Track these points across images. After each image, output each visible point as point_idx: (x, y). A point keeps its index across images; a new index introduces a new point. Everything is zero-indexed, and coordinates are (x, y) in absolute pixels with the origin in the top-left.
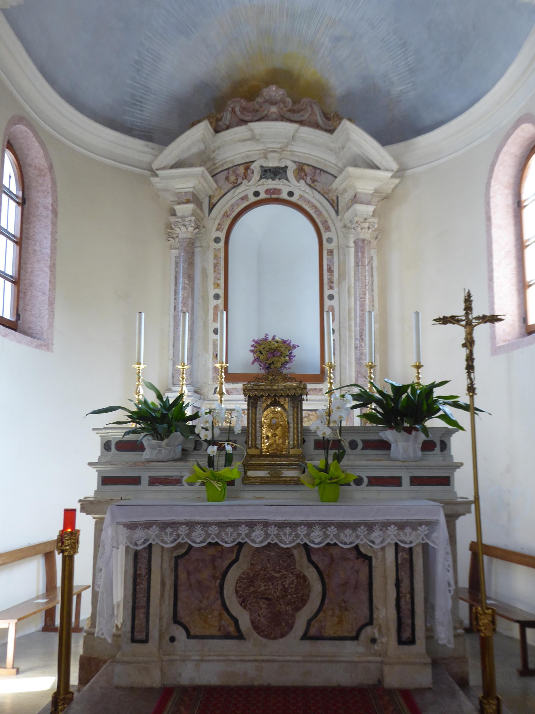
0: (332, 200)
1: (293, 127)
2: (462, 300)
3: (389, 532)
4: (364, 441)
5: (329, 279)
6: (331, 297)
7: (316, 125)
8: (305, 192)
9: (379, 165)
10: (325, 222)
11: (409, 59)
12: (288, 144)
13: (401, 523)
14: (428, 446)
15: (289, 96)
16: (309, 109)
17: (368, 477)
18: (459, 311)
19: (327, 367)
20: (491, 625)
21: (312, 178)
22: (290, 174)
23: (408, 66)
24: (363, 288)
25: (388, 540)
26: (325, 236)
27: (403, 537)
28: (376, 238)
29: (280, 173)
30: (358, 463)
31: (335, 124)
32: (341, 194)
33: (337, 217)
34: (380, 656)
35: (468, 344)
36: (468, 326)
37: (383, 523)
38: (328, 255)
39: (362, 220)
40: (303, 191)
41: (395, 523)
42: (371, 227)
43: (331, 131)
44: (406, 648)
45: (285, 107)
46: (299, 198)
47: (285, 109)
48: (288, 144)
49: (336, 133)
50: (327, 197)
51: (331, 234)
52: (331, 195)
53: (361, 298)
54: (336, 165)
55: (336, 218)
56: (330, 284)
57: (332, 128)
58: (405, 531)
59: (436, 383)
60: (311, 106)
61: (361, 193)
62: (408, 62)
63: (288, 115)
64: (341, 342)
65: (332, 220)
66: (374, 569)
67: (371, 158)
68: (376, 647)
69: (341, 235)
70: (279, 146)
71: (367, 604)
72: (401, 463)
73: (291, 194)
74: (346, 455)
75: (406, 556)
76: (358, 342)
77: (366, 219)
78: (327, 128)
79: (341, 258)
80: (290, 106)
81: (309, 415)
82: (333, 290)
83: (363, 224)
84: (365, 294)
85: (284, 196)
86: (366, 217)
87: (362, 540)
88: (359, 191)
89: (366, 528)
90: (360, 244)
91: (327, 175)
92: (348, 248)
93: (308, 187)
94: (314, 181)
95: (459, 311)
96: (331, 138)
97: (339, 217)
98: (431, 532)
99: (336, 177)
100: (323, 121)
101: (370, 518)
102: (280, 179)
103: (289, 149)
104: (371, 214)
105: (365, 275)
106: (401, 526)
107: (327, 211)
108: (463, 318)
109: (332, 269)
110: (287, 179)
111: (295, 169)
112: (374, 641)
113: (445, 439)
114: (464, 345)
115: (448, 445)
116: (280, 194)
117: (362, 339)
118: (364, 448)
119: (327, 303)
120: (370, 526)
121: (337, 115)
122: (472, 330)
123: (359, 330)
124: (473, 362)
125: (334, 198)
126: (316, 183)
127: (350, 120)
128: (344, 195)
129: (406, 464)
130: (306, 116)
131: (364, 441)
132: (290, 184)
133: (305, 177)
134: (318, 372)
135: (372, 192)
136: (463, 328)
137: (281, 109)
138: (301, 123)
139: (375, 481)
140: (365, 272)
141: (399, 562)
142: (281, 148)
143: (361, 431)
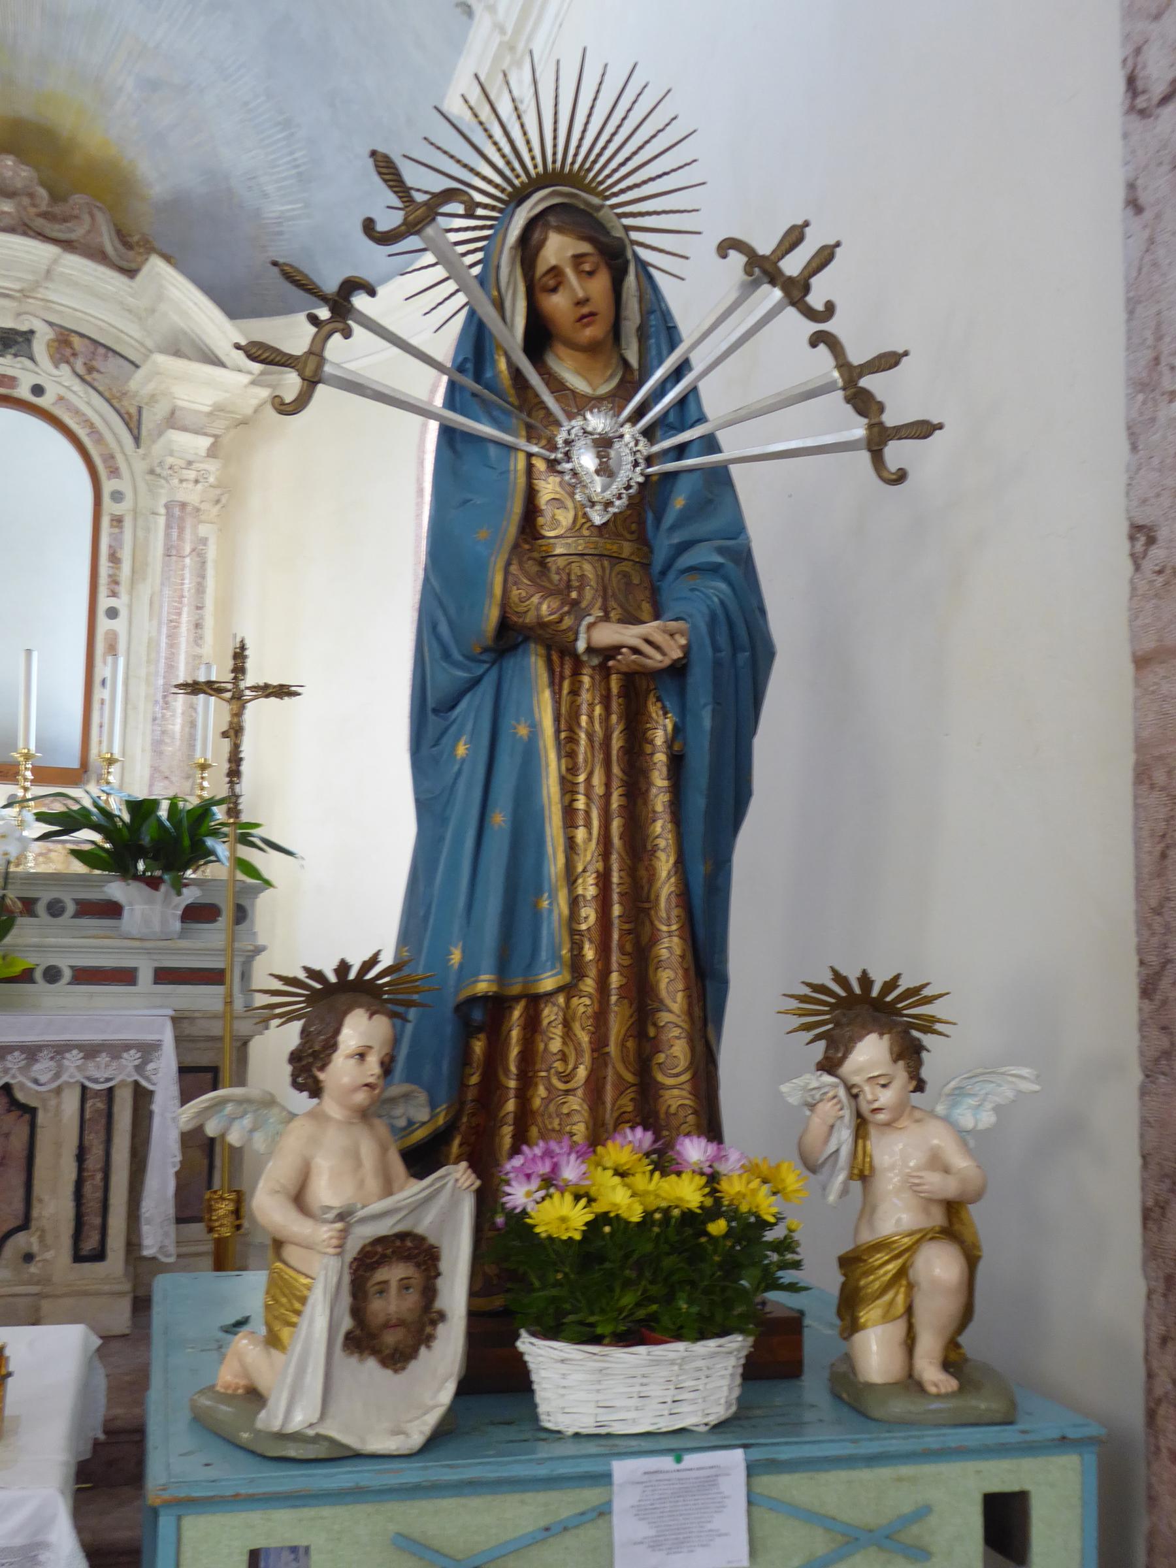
0: (128, 413)
1: (47, 251)
2: (230, 653)
3: (66, 1062)
4: (78, 902)
5: (110, 576)
6: (112, 613)
7: (99, 256)
8: (71, 390)
9: (224, 358)
10: (110, 458)
11: (296, 155)
12: (37, 285)
13: (91, 1045)
14: (200, 914)
15: (43, 184)
16: (86, 218)
17: (71, 967)
18: (220, 672)
19: (21, 756)
20: (232, 1218)
21: (87, 362)
22: (39, 347)
23: (297, 166)
24: (176, 602)
25: (65, 1078)
26: (108, 486)
27: (96, 1074)
28: (218, 501)
29: (16, 342)
30: (52, 941)
31: (139, 259)
32: (147, 404)
33: (138, 450)
34: (37, 1283)
35: (232, 733)
36: (234, 701)
37: (58, 1046)
38: (112, 526)
39: (182, 463)
40: (66, 387)
41: (80, 1047)
42: (201, 480)
43: (131, 273)
44: (87, 1266)
45: (34, 205)
46: (57, 401)
47: (33, 210)
48: (37, 285)
49: (140, 277)
50: (117, 405)
51: (122, 485)
52: (125, 403)
53: (171, 621)
54: (142, 344)
55: (136, 452)
56: (113, 586)
57: (133, 266)
58: (98, 1059)
59: (218, 797)
60: (92, 216)
61: (182, 409)
62: (295, 160)
63: (39, 223)
64: (129, 706)
65: (125, 454)
66: (39, 1131)
67: (208, 341)
68: (33, 1269)
69: (142, 487)
70: (17, 286)
71: (20, 1193)
72: (137, 944)
73: (38, 390)
74: (15, 927)
75: (101, 1105)
76: (157, 709)
77: (190, 463)
78: (125, 264)
79: (140, 534)
80: (44, 207)
81: (50, 851)
82: (118, 597)
83: (184, 471)
84: (179, 614)
85: (24, 392)
86: (191, 458)
87: (14, 1077)
88: (180, 403)
89: (24, 1056)
90: (177, 511)
91: (121, 361)
92: (157, 516)
93: (77, 381)
94: (91, 369)
95: (220, 672)
96: (131, 287)
97: (141, 451)
98: (145, 1061)
99: (137, 367)
100: (116, 249)
101: (31, 1038)
102: (16, 355)
103: (39, 296)
104: (203, 453)
105: (183, 575)
106: (91, 1051)
107: (115, 434)
108: (229, 686)
109: (118, 555)
110: (32, 358)
111: (50, 340)
112: (29, 1257)
113: (242, 902)
114: (225, 735)
115: (249, 912)
116: (13, 387)
117: (166, 703)
118: (78, 915)
119: (104, 624)
120: (31, 1052)
121: (147, 242)
122: (243, 707)
123: (163, 685)
124: (239, 765)
125: (133, 411)
126: (95, 375)
127: (168, 258)
128: (153, 407)
129: (148, 944)
130: (78, 232)
131: (78, 902)
132: (37, 369)
133: (72, 359)
134: (75, 764)
135: (207, 409)
136: (225, 704)
137: (25, 208)
138: (68, 245)
139: (86, 976)
140: (183, 570)
141: (87, 1116)
142: (20, 291)
143: (76, 883)
